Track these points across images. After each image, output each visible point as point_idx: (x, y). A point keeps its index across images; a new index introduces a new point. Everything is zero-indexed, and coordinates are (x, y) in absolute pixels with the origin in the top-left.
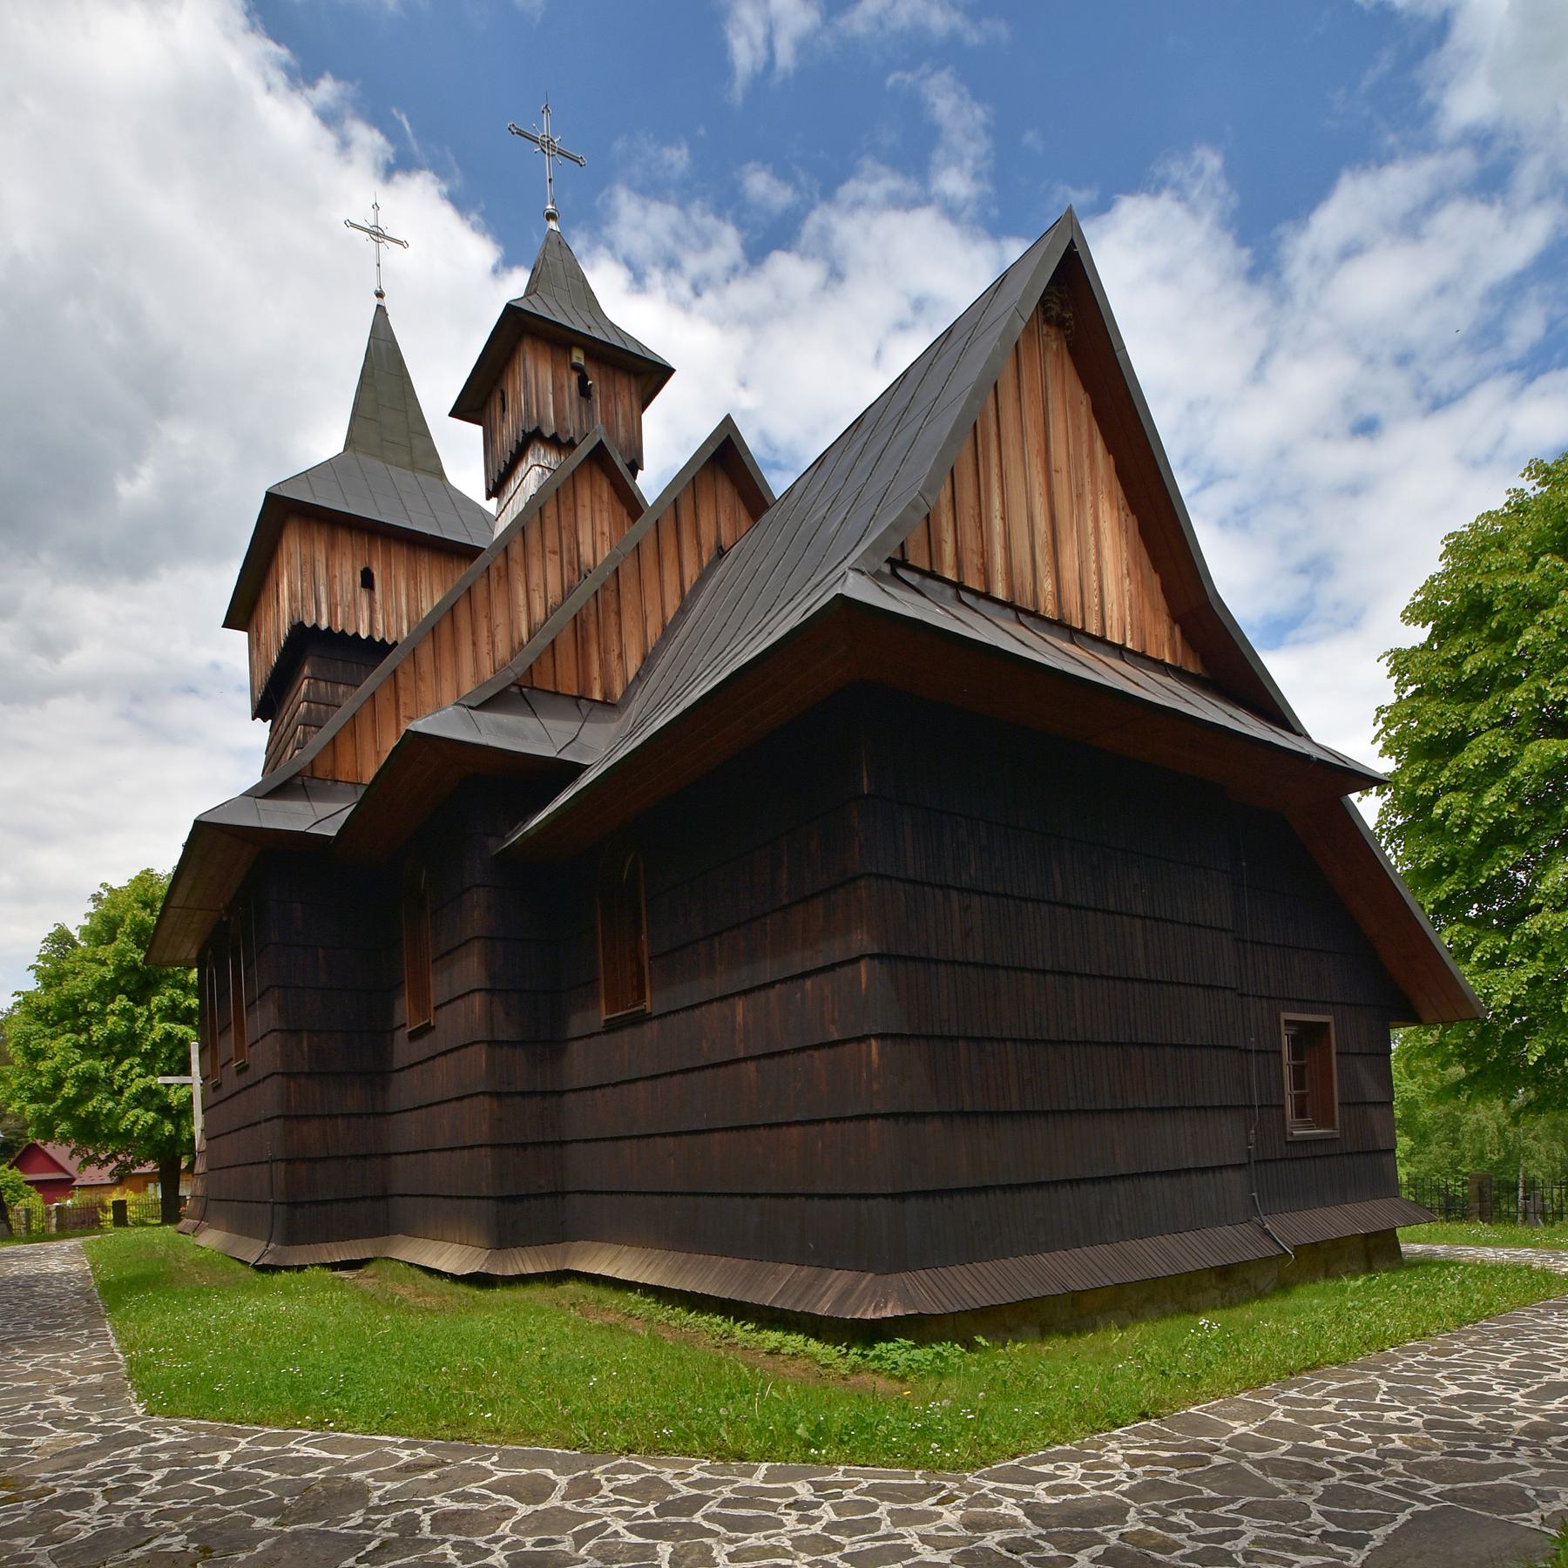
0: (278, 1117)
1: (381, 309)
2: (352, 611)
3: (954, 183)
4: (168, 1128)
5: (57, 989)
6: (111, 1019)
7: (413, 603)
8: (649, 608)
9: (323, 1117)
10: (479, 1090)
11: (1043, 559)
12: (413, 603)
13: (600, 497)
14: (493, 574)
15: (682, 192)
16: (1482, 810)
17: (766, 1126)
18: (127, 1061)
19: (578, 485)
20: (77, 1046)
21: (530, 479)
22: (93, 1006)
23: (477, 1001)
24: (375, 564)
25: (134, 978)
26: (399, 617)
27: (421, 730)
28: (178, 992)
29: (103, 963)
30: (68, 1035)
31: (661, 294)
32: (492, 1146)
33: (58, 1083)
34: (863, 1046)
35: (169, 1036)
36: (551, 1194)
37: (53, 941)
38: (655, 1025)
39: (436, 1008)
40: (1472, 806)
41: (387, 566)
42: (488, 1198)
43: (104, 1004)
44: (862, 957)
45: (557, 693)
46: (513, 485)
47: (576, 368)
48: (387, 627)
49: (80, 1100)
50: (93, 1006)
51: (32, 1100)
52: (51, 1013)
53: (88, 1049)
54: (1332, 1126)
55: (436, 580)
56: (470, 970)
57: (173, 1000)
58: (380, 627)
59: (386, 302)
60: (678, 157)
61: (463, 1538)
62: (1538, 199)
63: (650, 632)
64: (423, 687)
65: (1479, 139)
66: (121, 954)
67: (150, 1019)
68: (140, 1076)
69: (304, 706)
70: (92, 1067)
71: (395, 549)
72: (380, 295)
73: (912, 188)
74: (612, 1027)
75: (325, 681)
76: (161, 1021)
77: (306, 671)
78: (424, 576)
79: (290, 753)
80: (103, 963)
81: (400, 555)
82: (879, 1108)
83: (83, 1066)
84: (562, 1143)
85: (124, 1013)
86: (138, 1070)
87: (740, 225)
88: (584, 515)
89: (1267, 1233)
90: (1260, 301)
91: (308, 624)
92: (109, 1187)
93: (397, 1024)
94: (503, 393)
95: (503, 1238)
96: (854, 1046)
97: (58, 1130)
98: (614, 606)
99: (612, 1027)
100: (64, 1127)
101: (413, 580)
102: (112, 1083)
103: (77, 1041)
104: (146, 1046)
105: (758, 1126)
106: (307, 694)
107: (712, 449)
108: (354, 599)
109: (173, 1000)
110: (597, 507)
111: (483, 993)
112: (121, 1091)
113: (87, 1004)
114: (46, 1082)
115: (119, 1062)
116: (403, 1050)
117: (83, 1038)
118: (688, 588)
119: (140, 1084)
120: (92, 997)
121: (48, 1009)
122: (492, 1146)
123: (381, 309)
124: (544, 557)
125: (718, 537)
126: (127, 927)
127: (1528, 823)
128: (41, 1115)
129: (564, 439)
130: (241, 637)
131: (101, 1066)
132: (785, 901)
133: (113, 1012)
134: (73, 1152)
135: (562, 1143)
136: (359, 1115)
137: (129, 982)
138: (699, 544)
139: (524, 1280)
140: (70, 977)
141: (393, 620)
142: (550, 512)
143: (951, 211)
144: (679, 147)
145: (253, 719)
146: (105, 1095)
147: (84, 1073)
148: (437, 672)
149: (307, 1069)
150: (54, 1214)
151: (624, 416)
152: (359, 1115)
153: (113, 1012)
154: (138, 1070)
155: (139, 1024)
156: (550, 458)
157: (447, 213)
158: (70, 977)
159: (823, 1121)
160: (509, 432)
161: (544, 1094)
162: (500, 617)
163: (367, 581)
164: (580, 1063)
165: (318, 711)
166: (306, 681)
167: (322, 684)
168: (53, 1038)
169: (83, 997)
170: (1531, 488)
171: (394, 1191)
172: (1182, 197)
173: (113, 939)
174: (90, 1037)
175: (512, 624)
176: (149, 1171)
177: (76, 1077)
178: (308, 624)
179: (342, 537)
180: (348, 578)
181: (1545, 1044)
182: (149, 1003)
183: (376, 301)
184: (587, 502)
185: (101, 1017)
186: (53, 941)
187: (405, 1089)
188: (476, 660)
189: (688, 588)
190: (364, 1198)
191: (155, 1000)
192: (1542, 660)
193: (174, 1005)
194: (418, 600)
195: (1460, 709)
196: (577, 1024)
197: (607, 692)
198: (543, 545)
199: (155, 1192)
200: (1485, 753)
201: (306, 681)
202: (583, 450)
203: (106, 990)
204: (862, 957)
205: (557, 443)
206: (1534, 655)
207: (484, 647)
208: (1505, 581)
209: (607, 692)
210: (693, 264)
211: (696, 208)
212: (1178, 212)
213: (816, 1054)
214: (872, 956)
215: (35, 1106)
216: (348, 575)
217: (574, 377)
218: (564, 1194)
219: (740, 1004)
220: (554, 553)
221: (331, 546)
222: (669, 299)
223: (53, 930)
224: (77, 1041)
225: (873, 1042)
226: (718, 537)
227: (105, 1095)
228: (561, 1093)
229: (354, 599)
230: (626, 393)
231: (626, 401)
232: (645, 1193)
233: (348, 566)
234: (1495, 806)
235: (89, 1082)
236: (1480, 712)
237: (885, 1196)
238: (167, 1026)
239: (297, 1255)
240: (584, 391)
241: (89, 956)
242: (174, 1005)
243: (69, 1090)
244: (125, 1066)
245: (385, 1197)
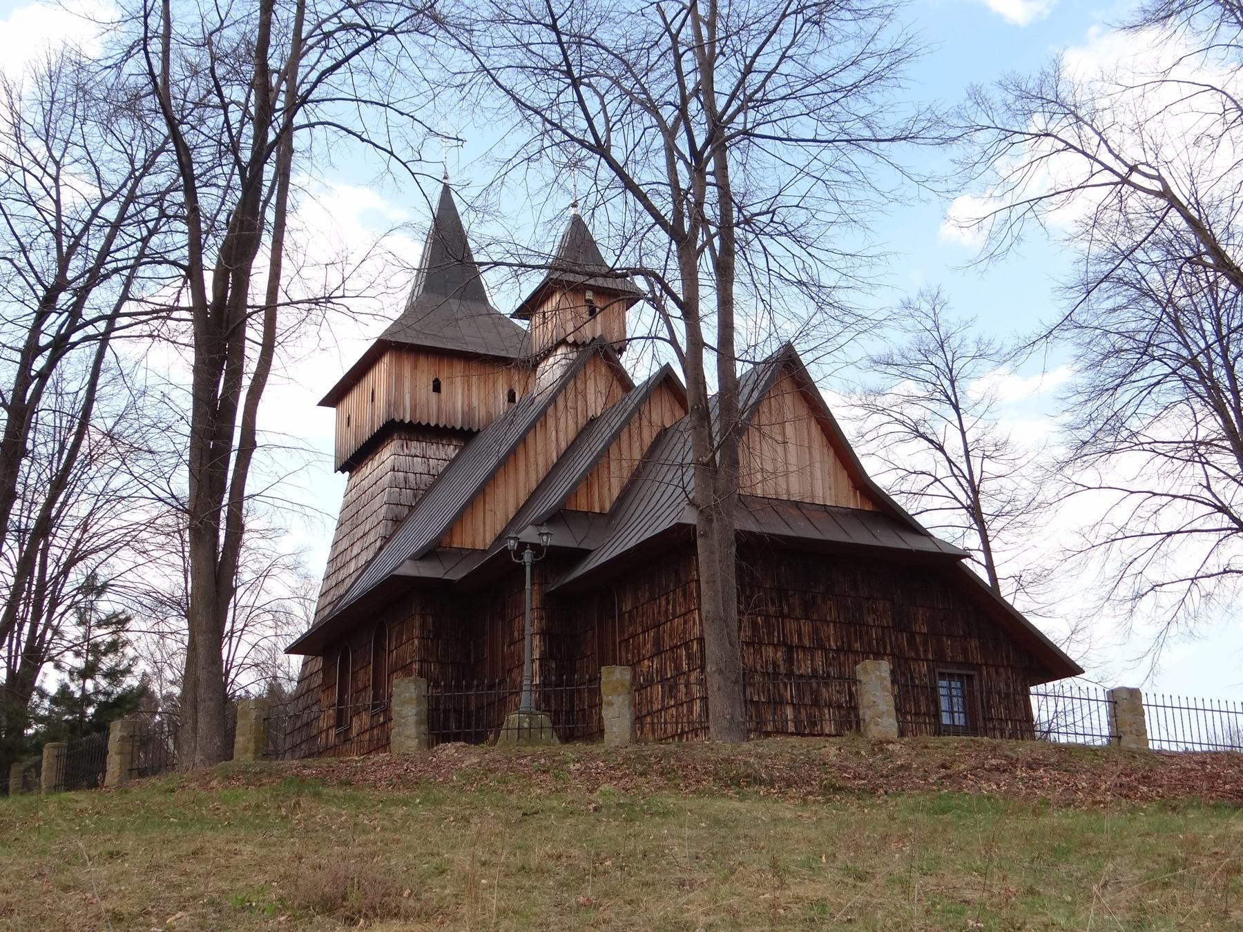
47: (587, 301)
78: (474, 380)
81: (459, 367)
88: (591, 384)
188: (527, 473)
221: (415, 367)
233: (424, 379)
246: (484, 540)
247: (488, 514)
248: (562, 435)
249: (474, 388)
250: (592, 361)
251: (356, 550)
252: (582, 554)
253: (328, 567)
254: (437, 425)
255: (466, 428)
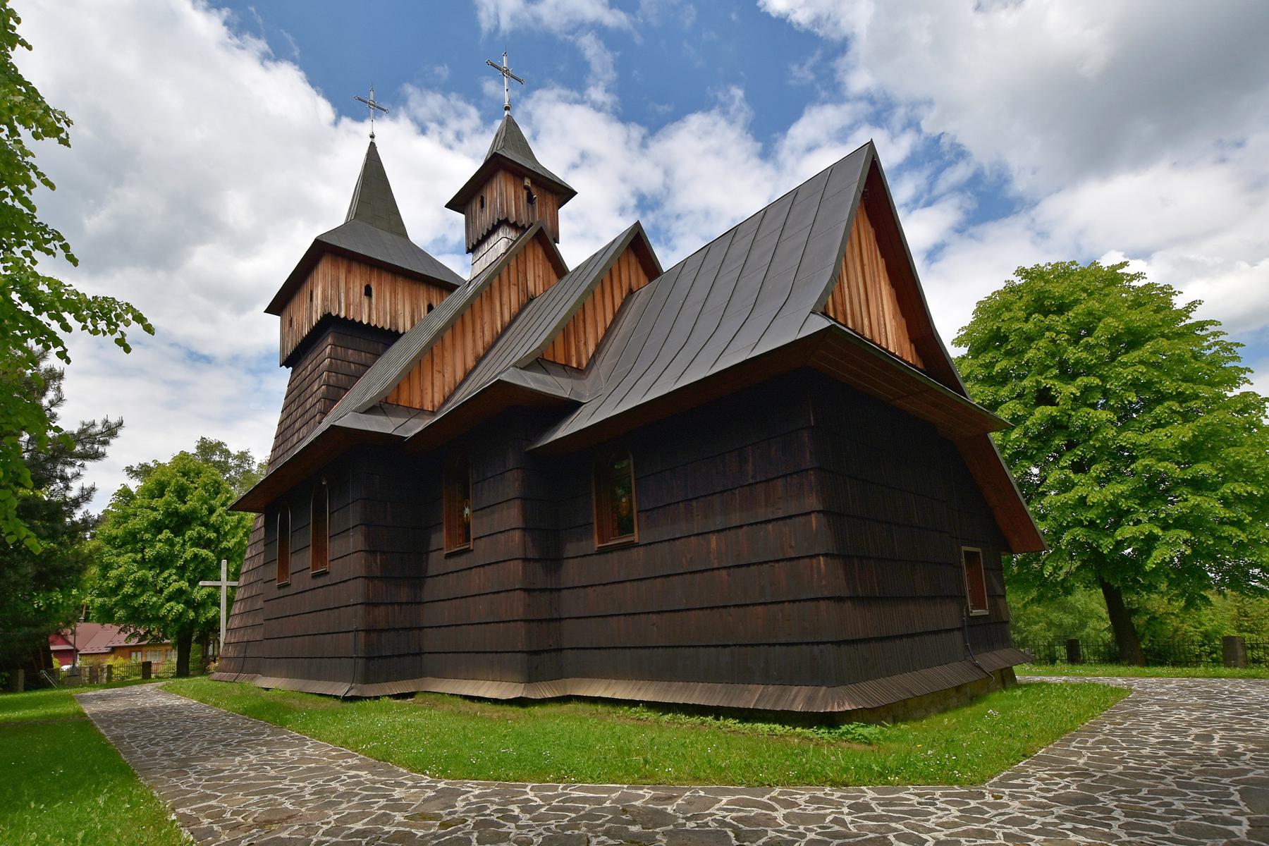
0: (362, 604)
1: (372, 145)
2: (359, 308)
3: (597, 94)
4: (192, 614)
5: (125, 525)
6: (159, 545)
7: (393, 305)
8: (598, 319)
9: (386, 604)
10: (517, 587)
11: (864, 309)
12: (393, 305)
13: (538, 257)
14: (484, 294)
15: (446, 89)
16: (1009, 441)
17: (735, 606)
18: (168, 571)
19: (527, 249)
20: (135, 561)
21: (499, 244)
22: (147, 536)
23: (517, 535)
24: (373, 283)
25: (175, 519)
26: (385, 314)
27: (505, 379)
28: (203, 528)
29: (154, 509)
30: (130, 554)
31: (436, 138)
32: (525, 621)
33: (121, 584)
34: (814, 561)
35: (196, 555)
36: (554, 650)
37: (120, 495)
38: (641, 550)
39: (474, 540)
40: (1003, 439)
41: (379, 284)
42: (523, 652)
43: (155, 536)
44: (813, 512)
45: (555, 362)
46: (486, 247)
47: (526, 188)
48: (378, 319)
49: (134, 596)
50: (147, 536)
51: (99, 596)
52: (118, 540)
53: (143, 563)
54: (985, 608)
55: (407, 295)
56: (511, 516)
57: (199, 533)
58: (374, 317)
59: (376, 141)
60: (443, 72)
61: (998, 801)
62: (904, 129)
63: (599, 332)
64: (446, 354)
65: (869, 98)
66: (168, 504)
67: (183, 545)
68: (175, 581)
69: (327, 361)
70: (144, 574)
71: (384, 275)
72: (372, 137)
73: (575, 95)
74: (602, 551)
75: (341, 347)
76: (191, 547)
77: (330, 340)
78: (399, 291)
79: (316, 387)
80: (154, 509)
81: (387, 279)
82: (826, 594)
83: (139, 574)
84: (560, 619)
85: (170, 542)
86: (174, 577)
87: (479, 107)
88: (530, 265)
89: (978, 667)
90: (769, 169)
91: (334, 314)
92: (104, 656)
93: (432, 548)
94: (482, 198)
95: (531, 677)
96: (807, 560)
97: (117, 615)
98: (582, 317)
99: (602, 551)
100: (120, 613)
101: (394, 293)
102: (156, 585)
103: (135, 558)
104: (181, 562)
105: (730, 606)
106: (330, 354)
107: (631, 238)
108: (360, 301)
109: (199, 533)
110: (536, 262)
111: (520, 530)
112: (161, 591)
113: (143, 535)
114: (112, 584)
115: (162, 572)
116: (435, 563)
117: (140, 555)
118: (616, 310)
119: (176, 586)
120: (146, 530)
121: (115, 538)
122: (525, 621)
123: (372, 145)
124: (509, 286)
125: (630, 284)
126: (172, 488)
127: (1035, 449)
128: (105, 605)
129: (520, 225)
130: (276, 319)
131: (150, 575)
132: (751, 481)
133: (160, 541)
134: (121, 630)
135: (560, 619)
136: (407, 603)
137: (171, 521)
138: (621, 286)
139: (543, 702)
140: (132, 518)
141: (381, 314)
142: (513, 263)
143: (598, 108)
144: (443, 66)
145: (281, 366)
146: (152, 593)
147: (139, 578)
148: (454, 345)
149: (379, 575)
150: (106, 670)
151: (550, 215)
152: (407, 603)
153: (160, 541)
154: (174, 577)
155: (177, 548)
156: (512, 235)
157: (308, 88)
158: (132, 518)
159: (784, 602)
160: (486, 218)
161: (551, 590)
162: (487, 318)
163: (368, 292)
164: (572, 572)
165: (337, 365)
166: (330, 347)
167: (339, 348)
168: (118, 555)
169: (140, 530)
170: (1018, 280)
171: (426, 650)
172: (724, 113)
173: (161, 495)
174: (144, 556)
175: (493, 322)
176: (134, 644)
177: (134, 581)
178: (334, 314)
179: (355, 267)
180: (357, 289)
181: (1053, 566)
182: (184, 535)
183: (370, 140)
184: (532, 259)
185: (151, 543)
186: (120, 495)
187: (432, 589)
188: (474, 341)
189: (616, 310)
190: (408, 655)
191: (189, 533)
192: (1036, 366)
193: (200, 537)
194: (396, 304)
195: (992, 389)
196: (571, 549)
197: (579, 363)
198: (509, 280)
199: (174, 658)
200: (1010, 412)
201: (330, 347)
202: (531, 232)
203: (157, 527)
204: (813, 512)
205: (514, 226)
206: (1032, 363)
207: (479, 334)
208: (1016, 326)
209: (579, 363)
210: (454, 124)
211: (453, 96)
212: (722, 123)
213: (777, 565)
214: (818, 512)
215: (101, 600)
216: (357, 288)
217: (525, 192)
218: (561, 650)
219: (714, 539)
220: (515, 285)
221: (349, 271)
222: (441, 141)
223: (120, 488)
224: (135, 558)
225: (821, 558)
226: (630, 284)
227: (152, 593)
228: (559, 590)
229: (360, 301)
230: (550, 203)
231: (551, 207)
232: (630, 648)
233: (357, 283)
234: (1016, 440)
235: (141, 584)
236: (1004, 392)
237: (832, 643)
238: (195, 550)
239: (372, 690)
240: (530, 199)
241: (145, 505)
242: (200, 537)
243: (128, 589)
244: (166, 574)
245: (420, 654)
246: (433, 401)
247: (436, 375)
248: (455, 362)
249: (400, 297)
250: (531, 245)
251: (297, 425)
252: (570, 407)
253: (276, 442)
254: (369, 324)
255: (393, 329)
